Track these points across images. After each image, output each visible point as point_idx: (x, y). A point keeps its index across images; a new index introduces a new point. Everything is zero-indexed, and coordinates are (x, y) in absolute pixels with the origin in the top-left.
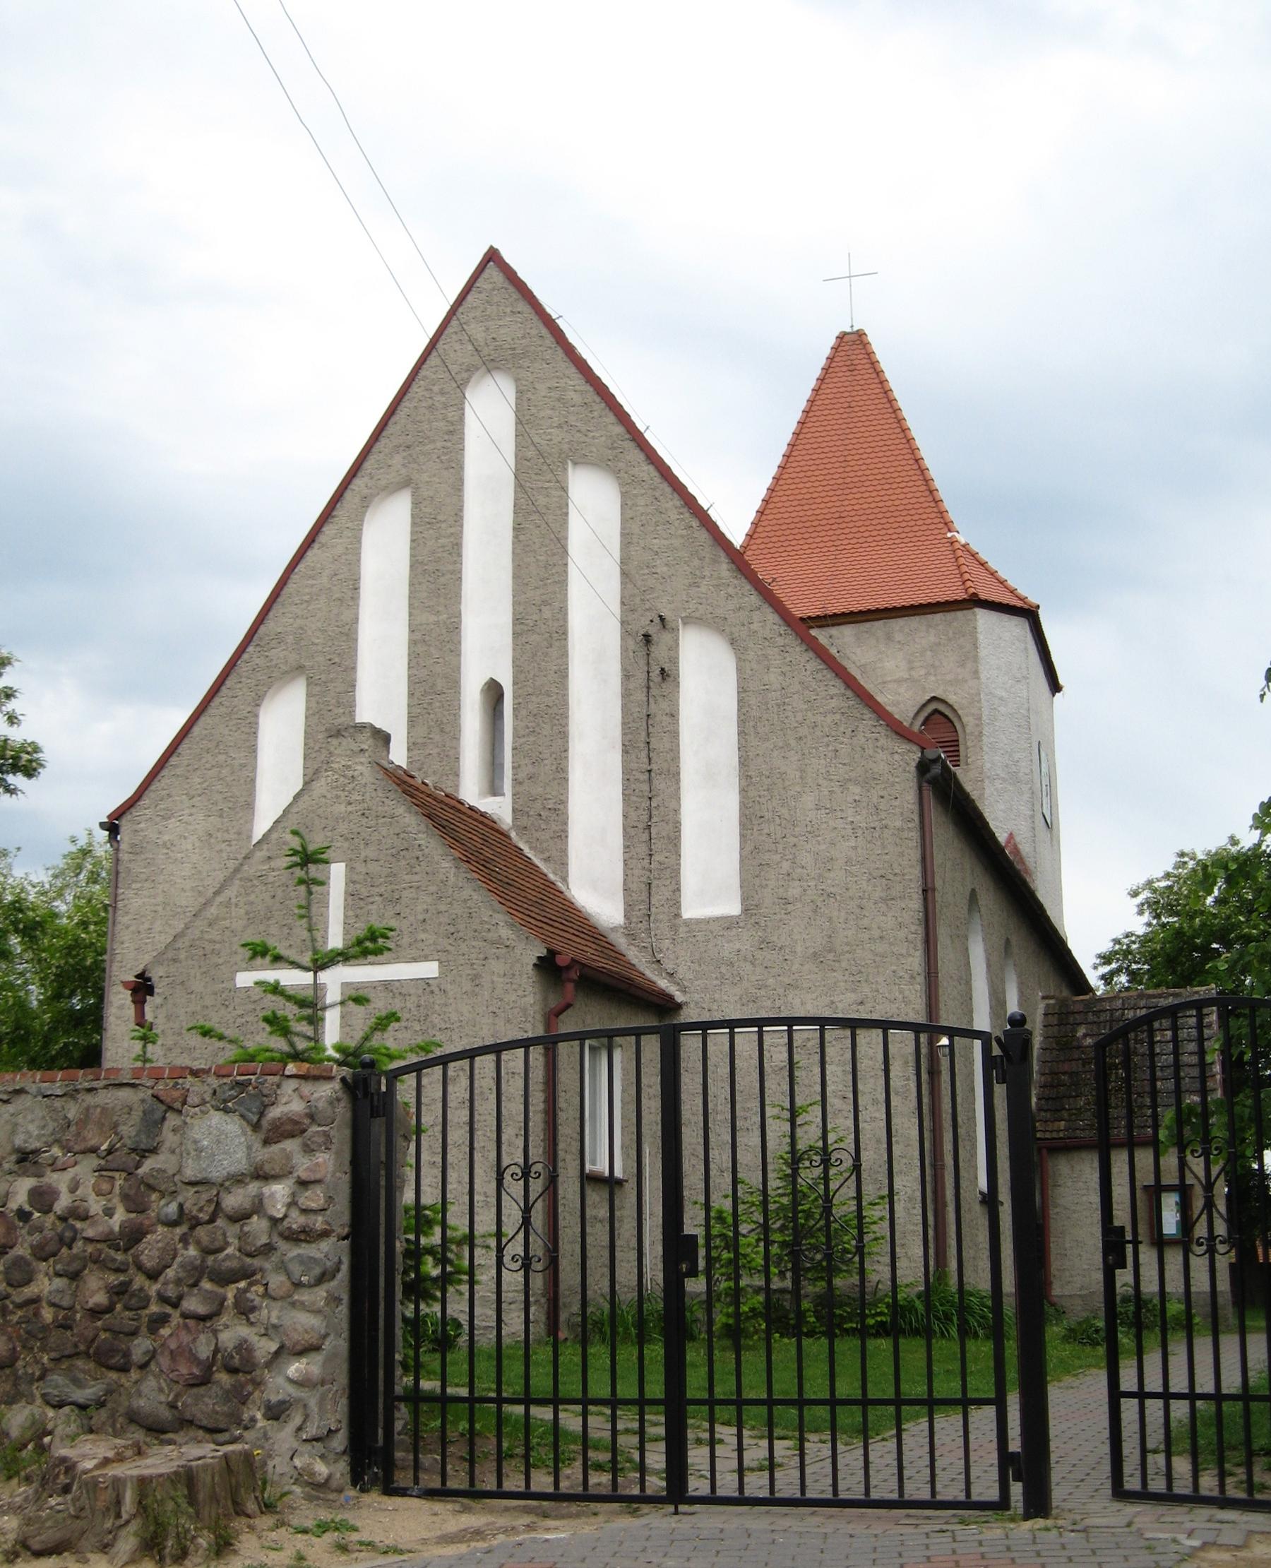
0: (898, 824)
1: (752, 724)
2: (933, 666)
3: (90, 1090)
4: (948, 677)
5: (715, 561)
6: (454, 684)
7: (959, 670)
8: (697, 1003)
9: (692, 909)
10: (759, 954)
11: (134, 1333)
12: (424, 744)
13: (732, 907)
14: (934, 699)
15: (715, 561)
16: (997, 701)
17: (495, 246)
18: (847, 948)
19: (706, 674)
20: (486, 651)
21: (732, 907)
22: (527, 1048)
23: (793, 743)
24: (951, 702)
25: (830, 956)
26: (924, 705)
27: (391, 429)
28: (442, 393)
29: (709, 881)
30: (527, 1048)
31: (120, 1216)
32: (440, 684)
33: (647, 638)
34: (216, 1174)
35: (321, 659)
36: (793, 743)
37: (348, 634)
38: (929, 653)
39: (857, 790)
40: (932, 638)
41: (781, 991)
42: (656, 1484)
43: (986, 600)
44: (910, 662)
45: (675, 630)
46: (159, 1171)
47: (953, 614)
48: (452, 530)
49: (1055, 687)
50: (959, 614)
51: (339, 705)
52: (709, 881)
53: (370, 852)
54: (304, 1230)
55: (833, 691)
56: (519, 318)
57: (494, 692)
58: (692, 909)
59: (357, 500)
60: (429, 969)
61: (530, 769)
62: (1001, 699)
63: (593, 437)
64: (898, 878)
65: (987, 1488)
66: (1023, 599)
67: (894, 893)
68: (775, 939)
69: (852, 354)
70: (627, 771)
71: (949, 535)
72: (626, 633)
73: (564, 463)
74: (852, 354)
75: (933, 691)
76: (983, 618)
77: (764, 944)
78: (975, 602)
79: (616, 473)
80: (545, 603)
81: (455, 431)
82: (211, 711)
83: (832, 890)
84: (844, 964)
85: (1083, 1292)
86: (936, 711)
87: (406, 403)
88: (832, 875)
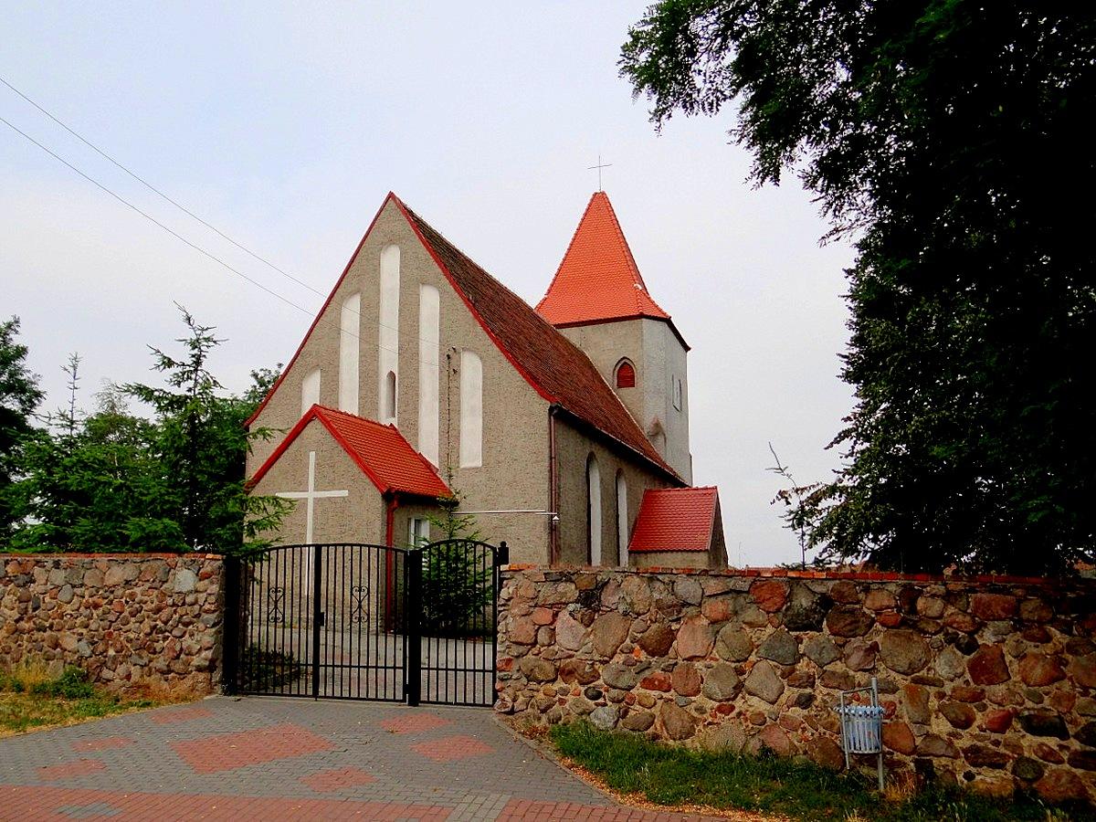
3: (148, 561)
5: (475, 325)
6: (377, 373)
9: (464, 464)
11: (158, 641)
13: (479, 463)
14: (624, 358)
15: (475, 325)
19: (472, 369)
20: (389, 361)
21: (479, 463)
26: (619, 362)
28: (372, 253)
29: (471, 453)
31: (156, 602)
33: (449, 357)
34: (184, 590)
37: (336, 352)
39: (525, 418)
40: (624, 332)
42: (310, 692)
45: (460, 353)
49: (687, 348)
51: (333, 381)
52: (471, 453)
53: (324, 448)
54: (209, 610)
57: (392, 375)
58: (464, 464)
60: (345, 493)
65: (399, 696)
66: (665, 314)
72: (441, 355)
78: (641, 316)
79: (438, 288)
81: (377, 268)
86: (625, 363)
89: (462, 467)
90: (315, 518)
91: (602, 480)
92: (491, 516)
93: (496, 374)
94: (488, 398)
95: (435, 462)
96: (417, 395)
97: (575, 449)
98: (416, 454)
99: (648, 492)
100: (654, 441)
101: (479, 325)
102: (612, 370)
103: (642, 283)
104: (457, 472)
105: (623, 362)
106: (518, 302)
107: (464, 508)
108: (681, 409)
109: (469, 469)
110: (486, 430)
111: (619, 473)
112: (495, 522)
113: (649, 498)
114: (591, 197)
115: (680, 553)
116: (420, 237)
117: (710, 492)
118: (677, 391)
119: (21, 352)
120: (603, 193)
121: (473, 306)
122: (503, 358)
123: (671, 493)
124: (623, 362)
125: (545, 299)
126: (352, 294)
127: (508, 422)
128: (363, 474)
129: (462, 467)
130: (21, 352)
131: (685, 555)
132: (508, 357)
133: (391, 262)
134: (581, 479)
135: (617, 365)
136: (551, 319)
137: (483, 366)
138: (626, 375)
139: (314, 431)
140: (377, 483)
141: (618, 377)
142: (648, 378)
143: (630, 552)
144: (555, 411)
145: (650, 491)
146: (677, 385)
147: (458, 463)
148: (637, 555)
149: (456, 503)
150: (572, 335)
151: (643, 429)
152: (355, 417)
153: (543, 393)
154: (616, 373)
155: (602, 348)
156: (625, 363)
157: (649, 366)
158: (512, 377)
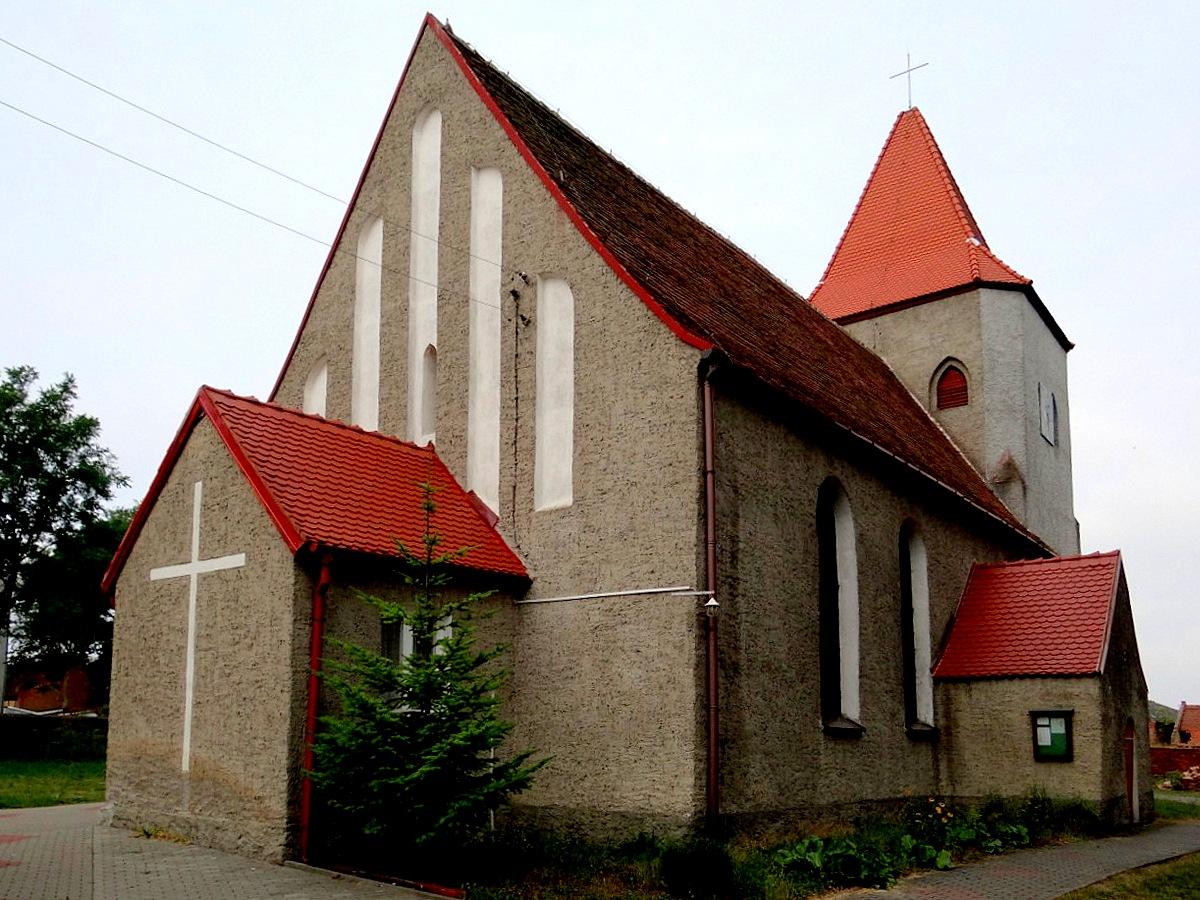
0: (683, 419)
1: (583, 351)
2: (948, 335)
4: (959, 341)
8: (542, 578)
10: (583, 536)
12: (388, 399)
13: (567, 500)
14: (949, 359)
17: (430, 12)
18: (643, 527)
20: (425, 328)
21: (567, 500)
23: (610, 361)
24: (960, 359)
25: (632, 534)
27: (372, 171)
29: (555, 482)
32: (397, 352)
33: (515, 294)
35: (334, 346)
36: (610, 361)
41: (597, 565)
43: (988, 282)
47: (962, 295)
48: (405, 237)
49: (1067, 346)
50: (967, 294)
52: (555, 482)
55: (639, 313)
56: (443, 64)
59: (354, 227)
60: (238, 560)
61: (445, 409)
62: (999, 352)
63: (487, 144)
64: (682, 465)
66: (1021, 278)
67: (679, 477)
68: (593, 523)
70: (503, 400)
71: (968, 240)
73: (468, 169)
75: (947, 352)
76: (985, 295)
77: (588, 528)
78: (978, 284)
80: (456, 281)
81: (406, 164)
82: (279, 393)
83: (634, 480)
84: (640, 541)
85: (980, 795)
86: (951, 367)
87: (380, 149)
88: (633, 467)
90: (199, 616)
91: (861, 539)
92: (612, 600)
93: (598, 312)
94: (583, 364)
95: (493, 504)
96: (466, 379)
97: (782, 470)
98: (463, 493)
99: (977, 572)
100: (1003, 493)
101: (568, 220)
102: (928, 380)
103: (978, 234)
104: (529, 520)
105: (946, 366)
106: (779, 292)
107: (539, 592)
108: (1058, 442)
109: (550, 512)
110: (581, 428)
111: (907, 535)
112: (596, 618)
113: (981, 578)
114: (895, 119)
115: (1038, 682)
116: (472, 81)
117: (1104, 561)
118: (1046, 411)
119: (86, 426)
121: (562, 190)
122: (611, 277)
123: (1026, 568)
124: (946, 366)
125: (819, 288)
126: (373, 217)
127: (619, 409)
128: (267, 517)
130: (86, 426)
131: (1051, 684)
132: (620, 274)
133: (428, 144)
134: (801, 532)
135: (936, 372)
136: (831, 311)
137: (576, 300)
138: (952, 384)
139: (202, 439)
140: (287, 530)
141: (938, 389)
142: (989, 392)
143: (937, 681)
144: (711, 369)
145: (983, 567)
146: (1046, 401)
147: (532, 501)
148: (951, 686)
149: (514, 586)
150: (861, 332)
151: (983, 474)
152: (321, 421)
153: (686, 327)
154: (935, 385)
155: (910, 351)
158: (628, 310)
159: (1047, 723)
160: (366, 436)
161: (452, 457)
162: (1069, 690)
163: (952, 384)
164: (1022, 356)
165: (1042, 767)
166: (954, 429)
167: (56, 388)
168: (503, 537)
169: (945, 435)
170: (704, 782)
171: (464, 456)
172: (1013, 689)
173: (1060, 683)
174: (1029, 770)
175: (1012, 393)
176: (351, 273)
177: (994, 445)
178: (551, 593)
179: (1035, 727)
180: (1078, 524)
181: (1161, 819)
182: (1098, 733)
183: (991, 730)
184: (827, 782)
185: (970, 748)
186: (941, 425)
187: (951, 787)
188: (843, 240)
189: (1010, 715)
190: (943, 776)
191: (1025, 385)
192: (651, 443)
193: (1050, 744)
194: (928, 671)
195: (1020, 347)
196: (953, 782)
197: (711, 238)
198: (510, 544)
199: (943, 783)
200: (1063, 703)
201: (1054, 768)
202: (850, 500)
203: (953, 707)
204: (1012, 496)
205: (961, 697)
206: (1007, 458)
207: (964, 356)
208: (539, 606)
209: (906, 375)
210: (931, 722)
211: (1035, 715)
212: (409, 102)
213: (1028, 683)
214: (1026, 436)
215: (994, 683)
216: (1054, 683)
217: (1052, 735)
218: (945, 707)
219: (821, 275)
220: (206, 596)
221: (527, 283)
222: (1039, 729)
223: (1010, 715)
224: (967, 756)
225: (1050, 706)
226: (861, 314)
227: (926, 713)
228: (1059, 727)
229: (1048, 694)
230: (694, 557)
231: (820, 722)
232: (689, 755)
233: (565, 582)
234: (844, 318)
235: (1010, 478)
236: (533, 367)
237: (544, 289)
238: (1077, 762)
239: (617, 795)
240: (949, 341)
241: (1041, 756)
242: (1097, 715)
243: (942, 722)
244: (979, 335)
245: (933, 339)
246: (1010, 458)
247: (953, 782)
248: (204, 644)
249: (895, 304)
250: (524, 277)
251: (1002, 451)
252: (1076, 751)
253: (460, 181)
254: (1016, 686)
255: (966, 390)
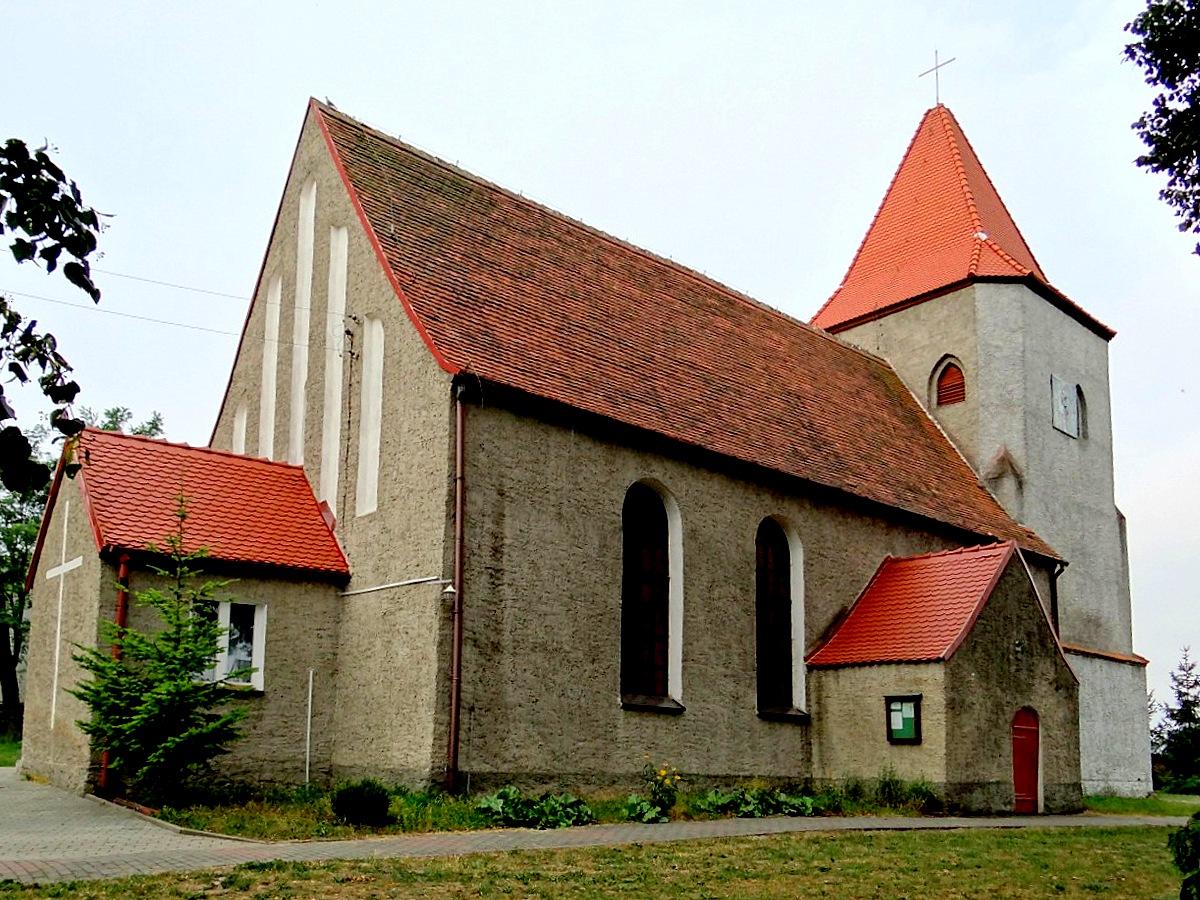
4: (957, 338)
7: (964, 332)
14: (947, 356)
16: (993, 349)
17: (9, 138)
21: (374, 509)
22: (892, 711)
27: (277, 233)
30: (892, 711)
38: (943, 324)
40: (946, 312)
44: (930, 332)
46: (546, 783)
49: (1106, 334)
62: (997, 347)
69: (940, 131)
71: (975, 235)
74: (940, 131)
75: (944, 349)
86: (950, 364)
89: (358, 515)
92: (394, 591)
100: (995, 489)
107: (355, 586)
110: (384, 443)
115: (893, 667)
120: (941, 106)
125: (838, 292)
129: (358, 515)
131: (905, 670)
135: (935, 369)
138: (949, 381)
141: (939, 387)
143: (810, 668)
156: (950, 364)
157: (987, 364)
159: (899, 707)
160: (236, 460)
161: (312, 473)
162: (919, 676)
163: (949, 381)
164: (1021, 349)
165: (896, 749)
166: (951, 426)
167: (146, 425)
168: (337, 540)
169: (943, 432)
170: (445, 742)
171: (319, 473)
172: (873, 675)
173: (911, 669)
174: (885, 753)
175: (1010, 388)
176: (262, 321)
177: (990, 440)
178: (362, 586)
179: (889, 711)
180: (1121, 518)
181: (93, 687)
182: (942, 717)
183: (854, 715)
184: (627, 753)
185: (836, 729)
186: (939, 423)
187: (821, 770)
188: (864, 243)
189: (869, 700)
190: (815, 759)
191: (1025, 378)
192: (422, 456)
193: (901, 728)
194: (802, 660)
195: (1021, 340)
196: (823, 765)
197: (637, 260)
198: (341, 546)
199: (815, 766)
200: (914, 688)
201: (906, 749)
202: (676, 499)
203: (824, 695)
204: (1005, 491)
205: (829, 679)
206: (1002, 454)
207: (960, 352)
208: (354, 597)
209: (907, 375)
210: (803, 708)
211: (889, 700)
212: (298, 174)
213: (884, 669)
214: (1025, 429)
215: (857, 668)
216: (907, 669)
217: (904, 719)
218: (816, 693)
219: (841, 279)
220: (66, 589)
221: (358, 323)
222: (893, 714)
223: (869, 700)
224: (835, 740)
225: (903, 692)
226: (865, 316)
227: (799, 701)
228: (908, 710)
229: (902, 679)
230: (442, 550)
231: (619, 699)
232: (431, 719)
233: (370, 576)
234: (835, 327)
235: (1003, 473)
236: (359, 394)
237: (371, 331)
238: (925, 745)
239: (389, 754)
240: (947, 338)
241: (894, 739)
242: (942, 700)
243: (814, 708)
244: (975, 330)
245: (932, 337)
246: (1007, 453)
247: (823, 765)
248: (64, 629)
249: (896, 305)
250: (355, 319)
251: (998, 446)
252: (924, 735)
253: (325, 239)
254: (874, 672)
255: (964, 387)
